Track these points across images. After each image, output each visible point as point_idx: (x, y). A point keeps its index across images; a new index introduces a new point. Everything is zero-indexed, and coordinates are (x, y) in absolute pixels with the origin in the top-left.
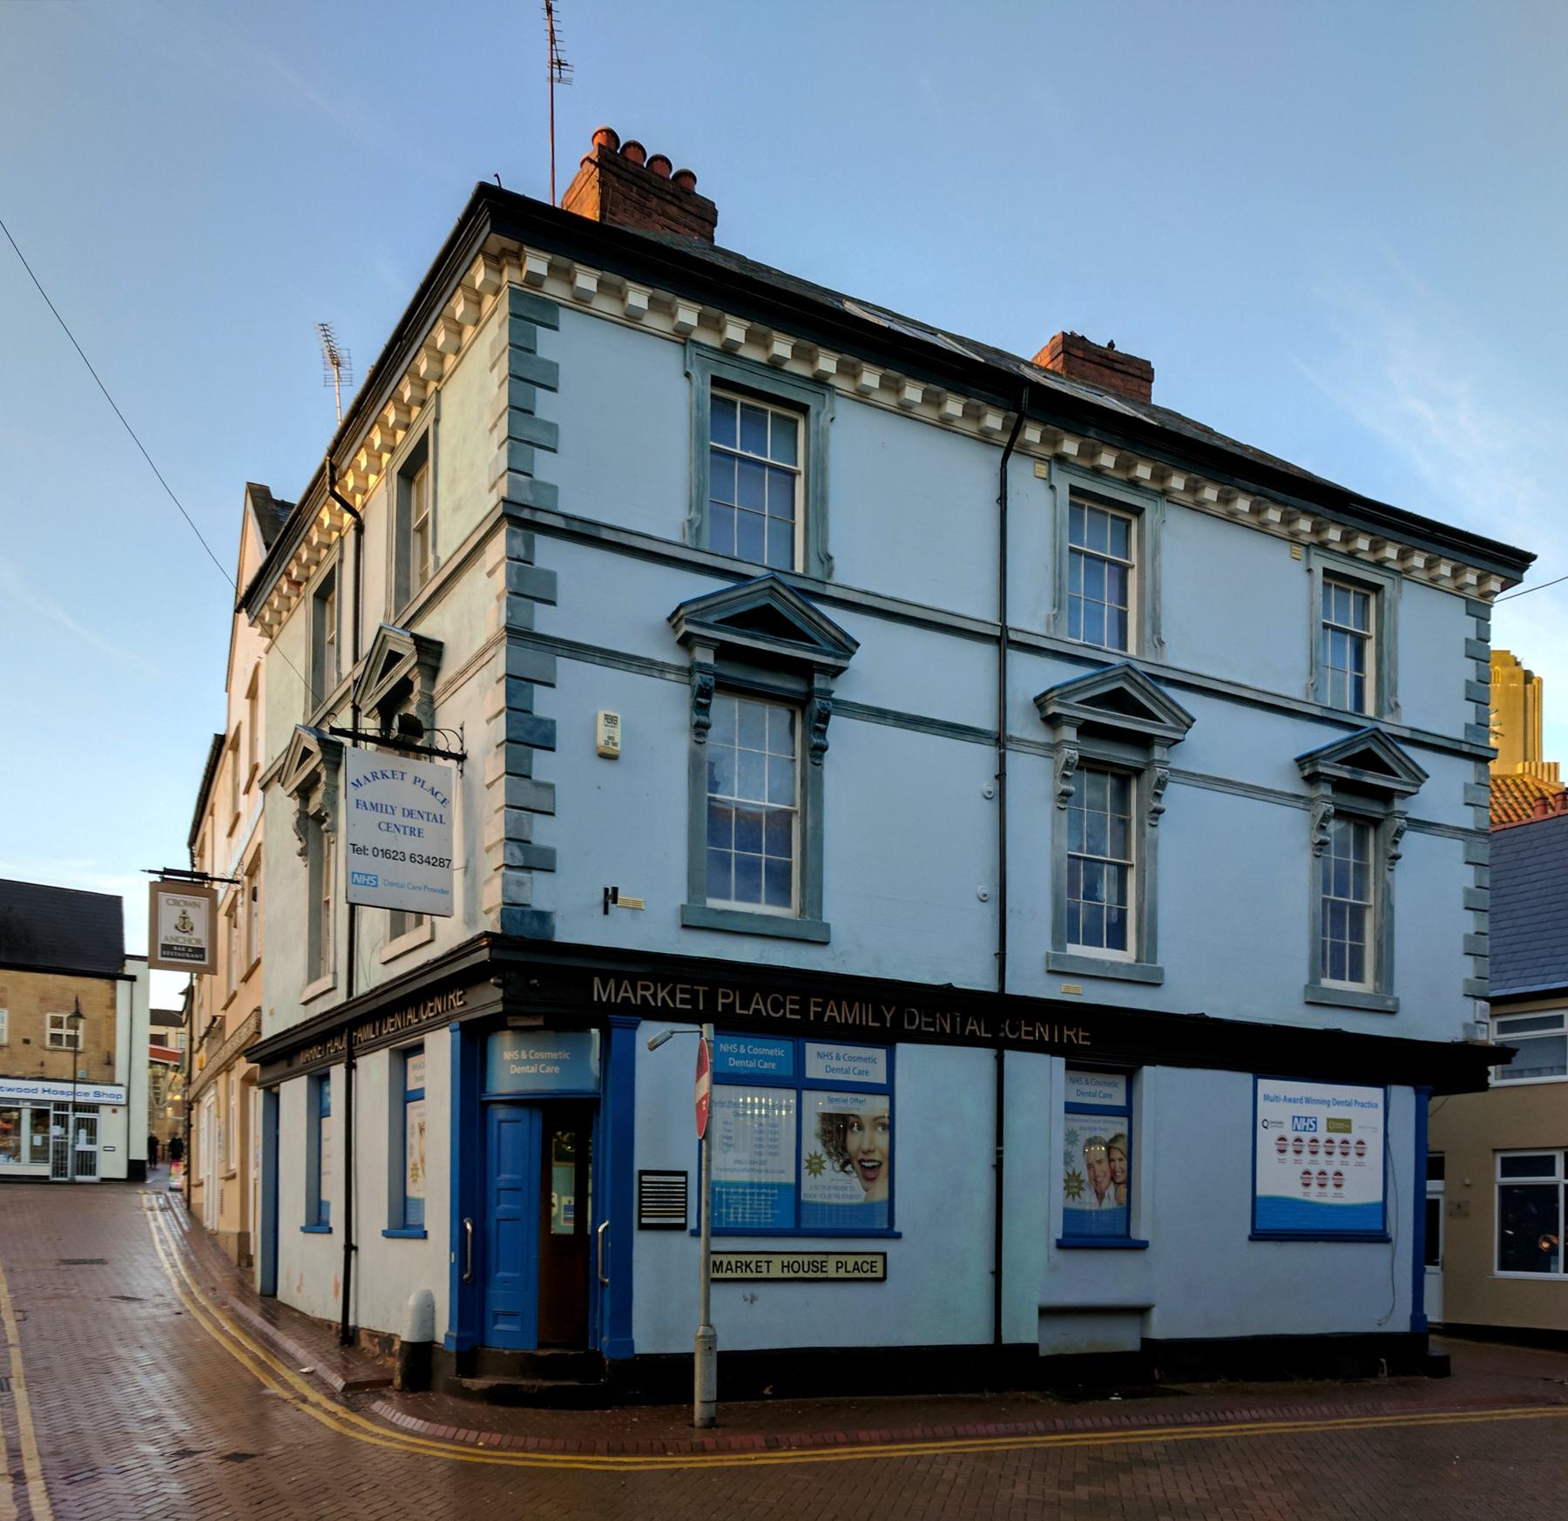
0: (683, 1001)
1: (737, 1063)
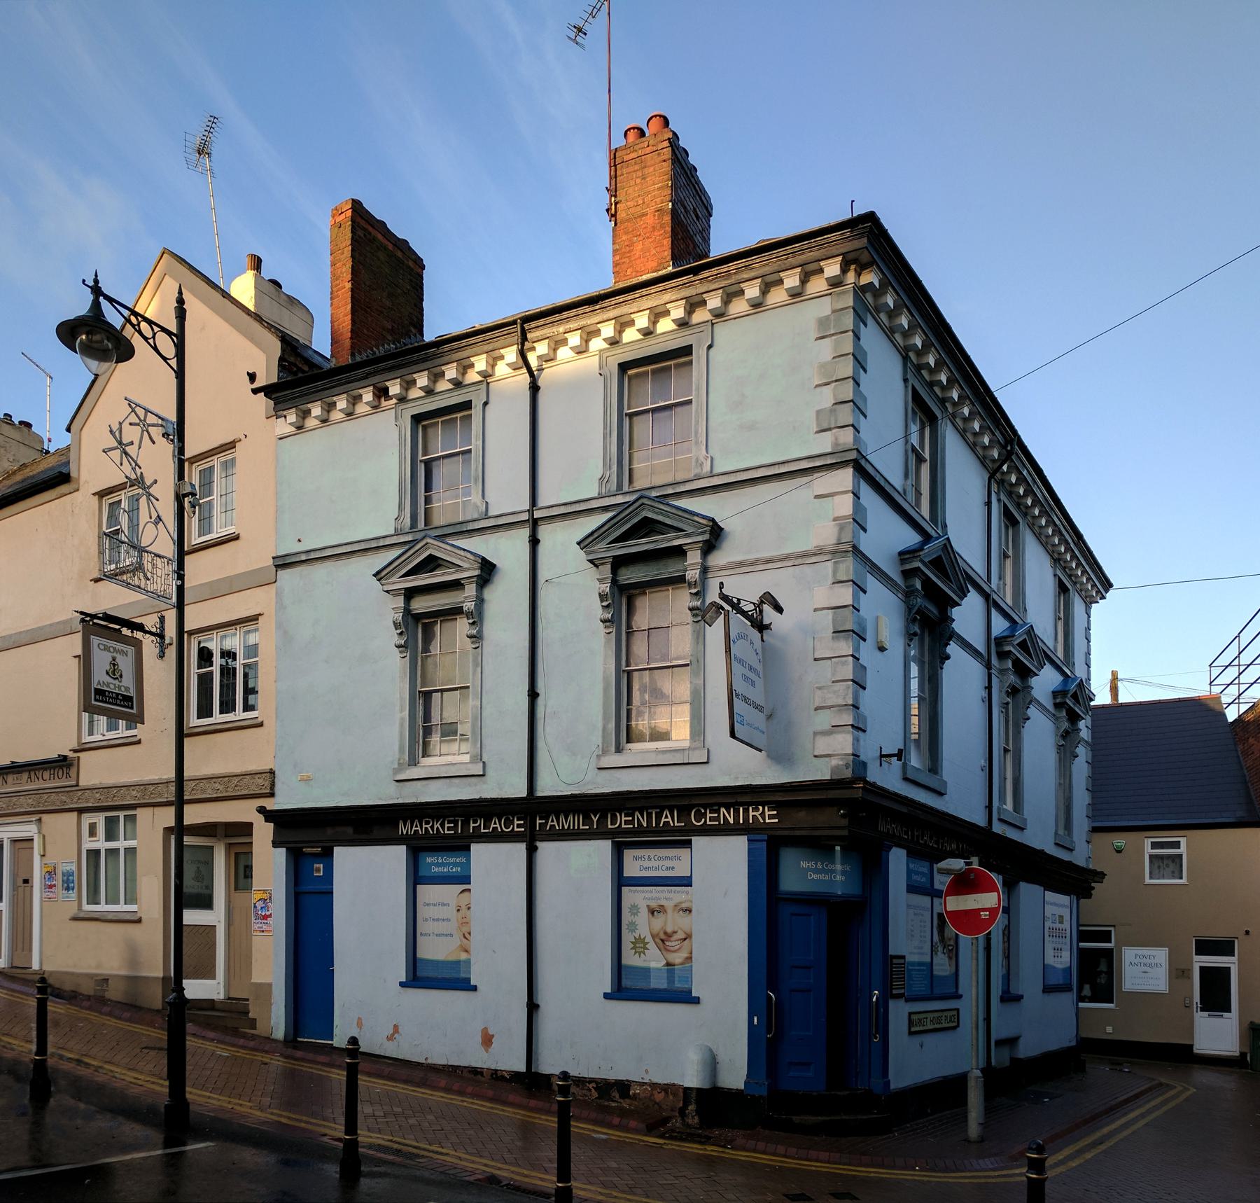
0: (449, 829)
1: (436, 869)
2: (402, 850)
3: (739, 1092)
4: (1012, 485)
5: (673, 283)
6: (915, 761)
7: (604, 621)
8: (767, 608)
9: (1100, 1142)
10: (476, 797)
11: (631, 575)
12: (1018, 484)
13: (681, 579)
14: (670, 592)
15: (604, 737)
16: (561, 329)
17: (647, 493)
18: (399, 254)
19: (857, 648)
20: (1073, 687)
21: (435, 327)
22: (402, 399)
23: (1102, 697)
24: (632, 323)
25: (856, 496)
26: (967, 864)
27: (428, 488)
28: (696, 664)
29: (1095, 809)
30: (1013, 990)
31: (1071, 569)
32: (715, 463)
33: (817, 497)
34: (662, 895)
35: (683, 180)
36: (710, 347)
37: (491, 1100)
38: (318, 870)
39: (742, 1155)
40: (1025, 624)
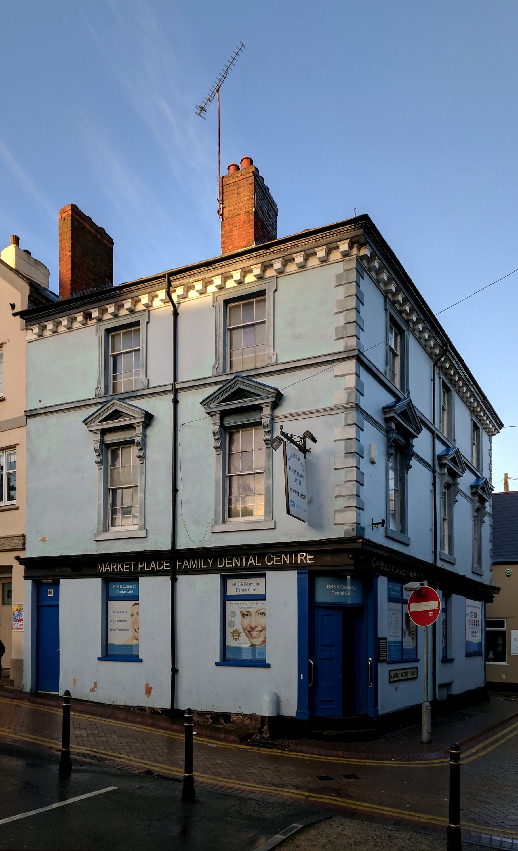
0: (126, 568)
1: (119, 592)
2: (99, 580)
3: (293, 718)
4: (447, 369)
5: (255, 254)
6: (392, 526)
7: (215, 448)
8: (308, 440)
9: (496, 741)
10: (142, 550)
11: (230, 421)
12: (450, 368)
13: (259, 424)
14: (253, 431)
15: (215, 515)
16: (191, 280)
17: (240, 374)
18: (99, 236)
19: (358, 462)
20: (481, 483)
21: (121, 276)
22: (100, 320)
23: (498, 488)
24: (231, 277)
25: (358, 376)
26: (421, 585)
27: (115, 370)
28: (267, 472)
29: (495, 552)
30: (449, 656)
31: (481, 416)
32: (278, 357)
33: (336, 376)
34: (248, 606)
35: (261, 195)
36: (275, 291)
37: (151, 725)
38: (51, 593)
39: (293, 755)
40: (455, 447)
